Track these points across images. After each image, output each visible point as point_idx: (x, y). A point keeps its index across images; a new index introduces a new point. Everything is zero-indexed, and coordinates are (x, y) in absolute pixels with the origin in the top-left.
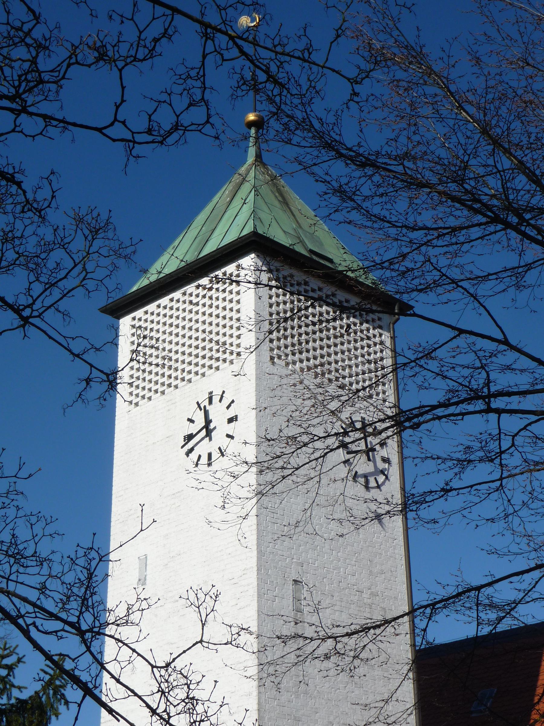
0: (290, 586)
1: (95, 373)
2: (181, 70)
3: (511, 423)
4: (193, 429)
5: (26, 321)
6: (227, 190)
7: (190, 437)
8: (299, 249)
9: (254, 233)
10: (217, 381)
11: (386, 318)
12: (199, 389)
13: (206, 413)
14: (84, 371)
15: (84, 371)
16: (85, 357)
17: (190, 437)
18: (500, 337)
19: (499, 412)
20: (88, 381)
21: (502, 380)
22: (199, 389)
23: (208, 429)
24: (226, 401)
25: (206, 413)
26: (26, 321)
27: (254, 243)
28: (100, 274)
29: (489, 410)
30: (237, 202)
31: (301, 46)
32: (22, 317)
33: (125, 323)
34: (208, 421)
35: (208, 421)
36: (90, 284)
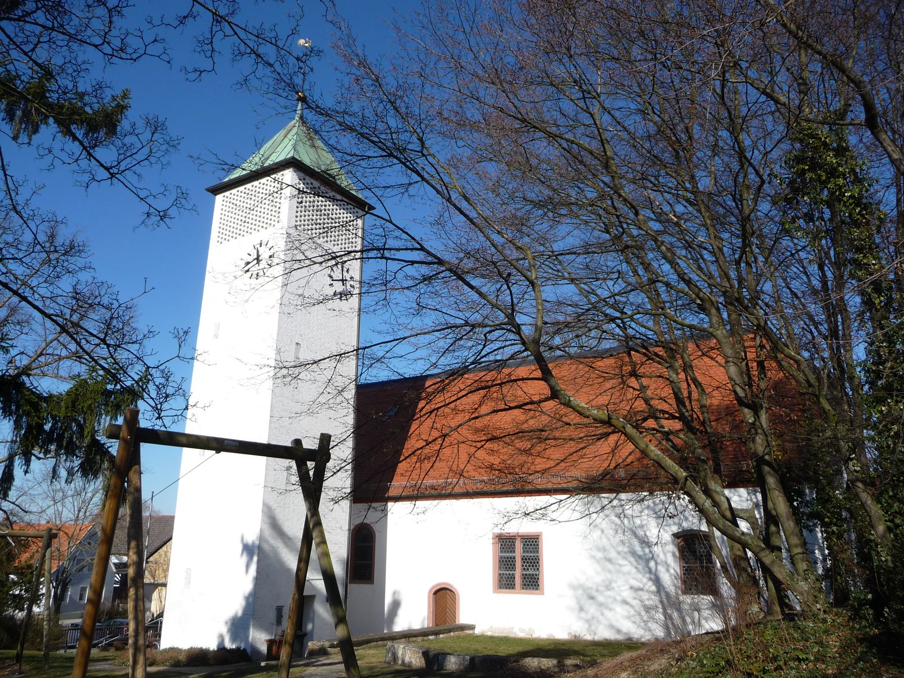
0: (294, 346)
1: (152, 210)
2: (201, 38)
3: (393, 266)
4: (250, 259)
5: (113, 175)
6: (282, 133)
7: (248, 263)
8: (316, 169)
9: (293, 158)
10: (263, 235)
11: (361, 213)
12: (255, 238)
13: (258, 251)
14: (146, 208)
15: (146, 208)
16: (147, 200)
17: (248, 263)
18: (388, 218)
19: (387, 259)
20: (148, 214)
21: (391, 243)
22: (255, 238)
23: (258, 259)
24: (269, 246)
25: (258, 251)
26: (113, 175)
27: (293, 163)
28: (159, 154)
29: (382, 257)
30: (286, 140)
31: (273, 34)
32: (110, 173)
33: (219, 198)
34: (258, 256)
35: (258, 256)
36: (152, 159)
